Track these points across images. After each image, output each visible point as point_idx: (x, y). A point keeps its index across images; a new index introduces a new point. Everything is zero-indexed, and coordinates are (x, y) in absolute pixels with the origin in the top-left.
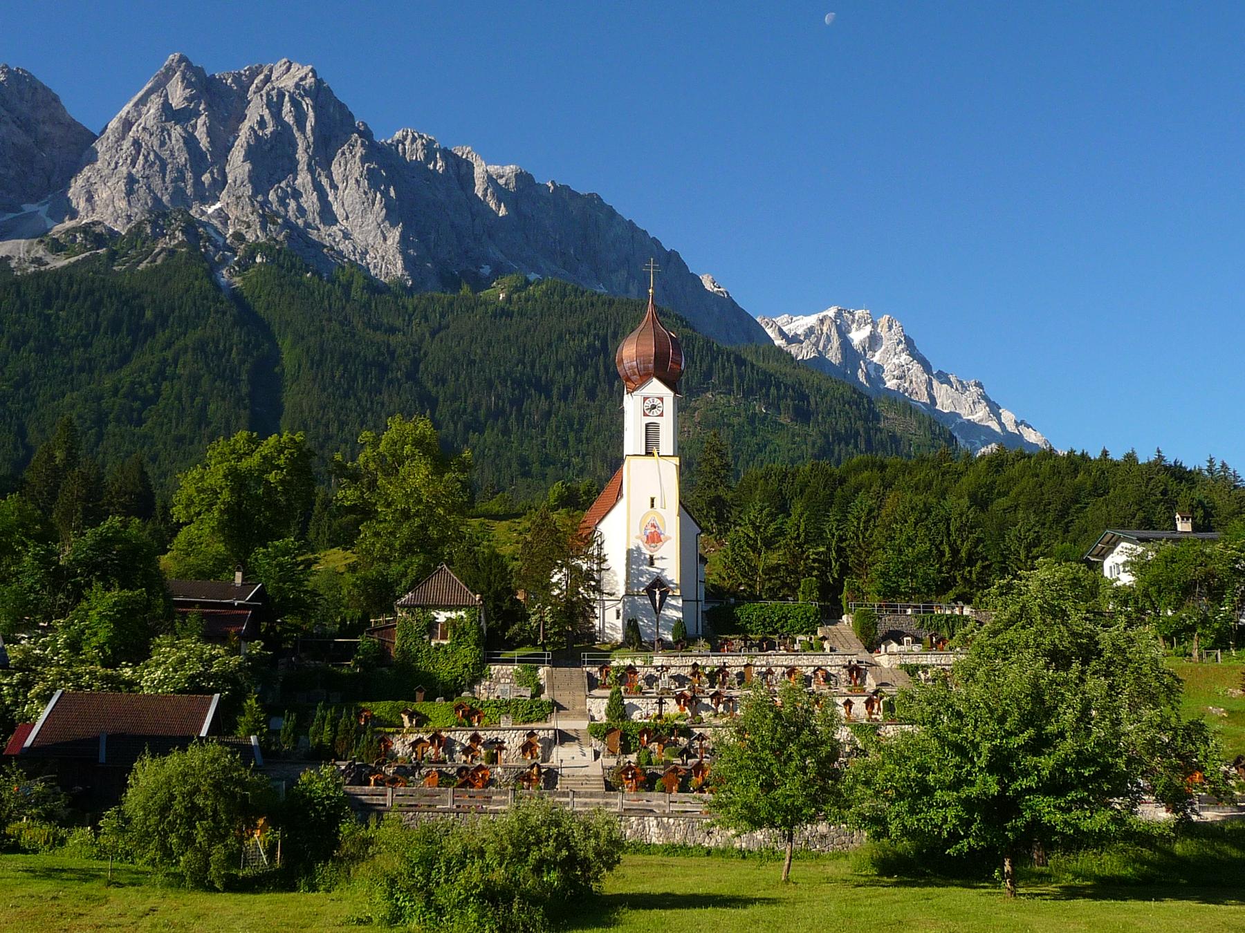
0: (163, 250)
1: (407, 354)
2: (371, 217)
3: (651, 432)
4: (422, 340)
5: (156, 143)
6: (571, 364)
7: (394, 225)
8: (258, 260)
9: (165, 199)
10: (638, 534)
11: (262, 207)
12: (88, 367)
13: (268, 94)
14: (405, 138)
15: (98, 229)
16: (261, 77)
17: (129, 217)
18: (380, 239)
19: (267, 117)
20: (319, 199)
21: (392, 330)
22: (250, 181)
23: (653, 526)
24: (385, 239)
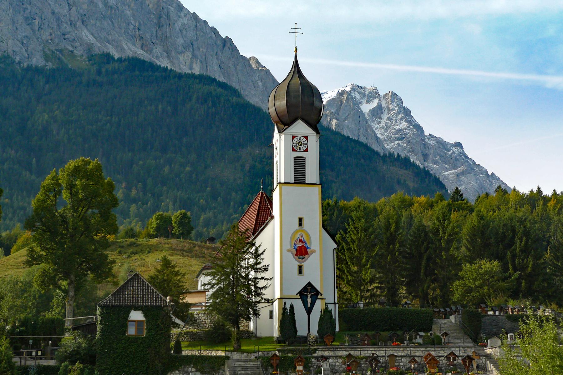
3: (299, 165)
10: (289, 247)
23: (301, 241)
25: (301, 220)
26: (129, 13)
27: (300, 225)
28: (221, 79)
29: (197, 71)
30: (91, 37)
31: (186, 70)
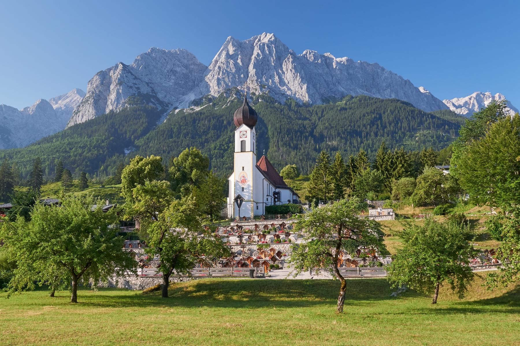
0: (229, 101)
1: (310, 127)
2: (296, 82)
3: (243, 143)
4: (315, 122)
5: (225, 67)
6: (368, 124)
7: (304, 84)
8: (260, 101)
9: (230, 84)
11: (260, 83)
12: (207, 141)
13: (259, 45)
14: (307, 53)
15: (210, 97)
16: (257, 40)
17: (219, 92)
18: (300, 89)
19: (260, 53)
20: (279, 78)
21: (305, 119)
22: (256, 75)
24: (302, 89)
25: (243, 168)
26: (359, 75)
27: (243, 170)
28: (405, 100)
29: (393, 96)
30: (342, 89)
31: (387, 97)
